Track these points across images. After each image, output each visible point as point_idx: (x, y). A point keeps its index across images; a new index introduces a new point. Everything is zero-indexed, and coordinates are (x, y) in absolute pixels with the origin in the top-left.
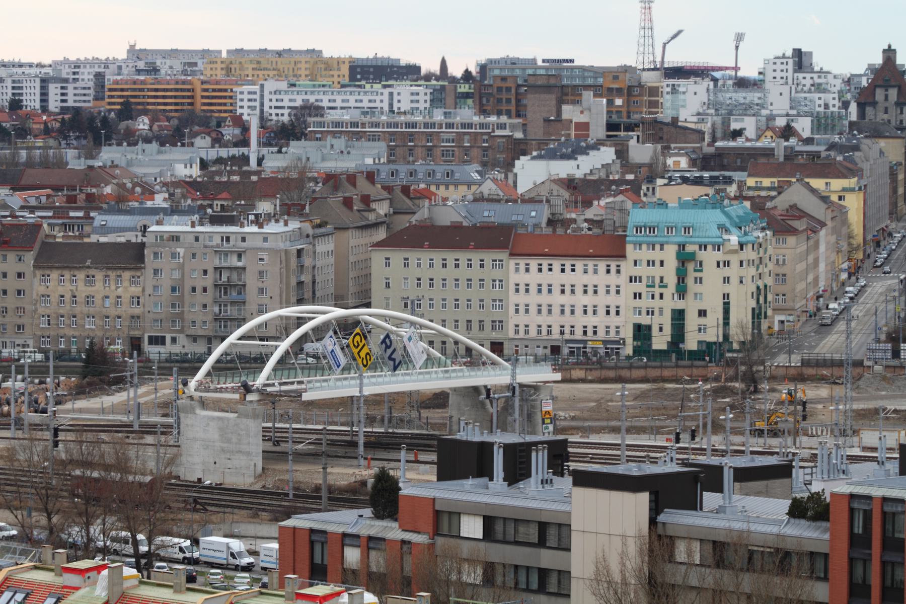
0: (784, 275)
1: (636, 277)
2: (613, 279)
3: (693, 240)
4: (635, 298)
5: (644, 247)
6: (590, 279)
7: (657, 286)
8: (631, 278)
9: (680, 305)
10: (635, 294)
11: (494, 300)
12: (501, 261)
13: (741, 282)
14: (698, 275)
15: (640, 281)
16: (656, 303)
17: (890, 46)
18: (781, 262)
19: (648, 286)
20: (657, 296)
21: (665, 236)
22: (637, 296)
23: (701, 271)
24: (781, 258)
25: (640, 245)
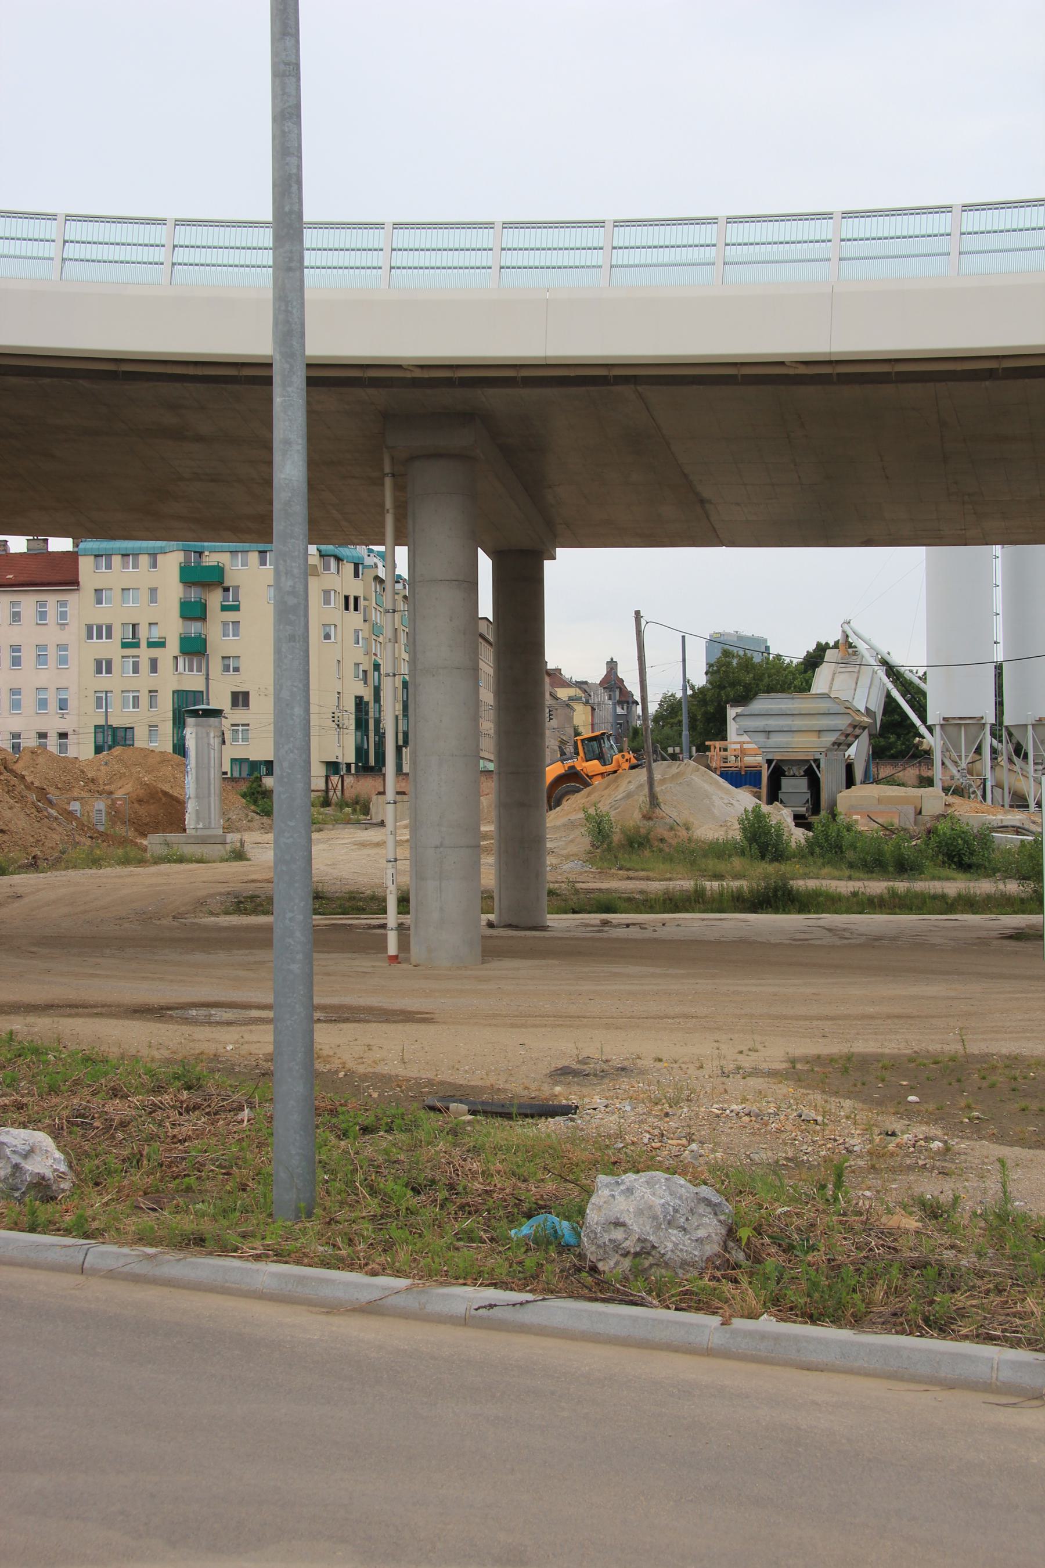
1: (99, 628)
2: (51, 635)
4: (99, 671)
5: (117, 560)
7: (144, 644)
8: (89, 628)
9: (194, 682)
10: (98, 663)
13: (327, 636)
14: (231, 616)
16: (145, 681)
17: (612, 659)
19: (125, 645)
20: (145, 666)
22: (104, 666)
23: (236, 608)
25: (109, 556)
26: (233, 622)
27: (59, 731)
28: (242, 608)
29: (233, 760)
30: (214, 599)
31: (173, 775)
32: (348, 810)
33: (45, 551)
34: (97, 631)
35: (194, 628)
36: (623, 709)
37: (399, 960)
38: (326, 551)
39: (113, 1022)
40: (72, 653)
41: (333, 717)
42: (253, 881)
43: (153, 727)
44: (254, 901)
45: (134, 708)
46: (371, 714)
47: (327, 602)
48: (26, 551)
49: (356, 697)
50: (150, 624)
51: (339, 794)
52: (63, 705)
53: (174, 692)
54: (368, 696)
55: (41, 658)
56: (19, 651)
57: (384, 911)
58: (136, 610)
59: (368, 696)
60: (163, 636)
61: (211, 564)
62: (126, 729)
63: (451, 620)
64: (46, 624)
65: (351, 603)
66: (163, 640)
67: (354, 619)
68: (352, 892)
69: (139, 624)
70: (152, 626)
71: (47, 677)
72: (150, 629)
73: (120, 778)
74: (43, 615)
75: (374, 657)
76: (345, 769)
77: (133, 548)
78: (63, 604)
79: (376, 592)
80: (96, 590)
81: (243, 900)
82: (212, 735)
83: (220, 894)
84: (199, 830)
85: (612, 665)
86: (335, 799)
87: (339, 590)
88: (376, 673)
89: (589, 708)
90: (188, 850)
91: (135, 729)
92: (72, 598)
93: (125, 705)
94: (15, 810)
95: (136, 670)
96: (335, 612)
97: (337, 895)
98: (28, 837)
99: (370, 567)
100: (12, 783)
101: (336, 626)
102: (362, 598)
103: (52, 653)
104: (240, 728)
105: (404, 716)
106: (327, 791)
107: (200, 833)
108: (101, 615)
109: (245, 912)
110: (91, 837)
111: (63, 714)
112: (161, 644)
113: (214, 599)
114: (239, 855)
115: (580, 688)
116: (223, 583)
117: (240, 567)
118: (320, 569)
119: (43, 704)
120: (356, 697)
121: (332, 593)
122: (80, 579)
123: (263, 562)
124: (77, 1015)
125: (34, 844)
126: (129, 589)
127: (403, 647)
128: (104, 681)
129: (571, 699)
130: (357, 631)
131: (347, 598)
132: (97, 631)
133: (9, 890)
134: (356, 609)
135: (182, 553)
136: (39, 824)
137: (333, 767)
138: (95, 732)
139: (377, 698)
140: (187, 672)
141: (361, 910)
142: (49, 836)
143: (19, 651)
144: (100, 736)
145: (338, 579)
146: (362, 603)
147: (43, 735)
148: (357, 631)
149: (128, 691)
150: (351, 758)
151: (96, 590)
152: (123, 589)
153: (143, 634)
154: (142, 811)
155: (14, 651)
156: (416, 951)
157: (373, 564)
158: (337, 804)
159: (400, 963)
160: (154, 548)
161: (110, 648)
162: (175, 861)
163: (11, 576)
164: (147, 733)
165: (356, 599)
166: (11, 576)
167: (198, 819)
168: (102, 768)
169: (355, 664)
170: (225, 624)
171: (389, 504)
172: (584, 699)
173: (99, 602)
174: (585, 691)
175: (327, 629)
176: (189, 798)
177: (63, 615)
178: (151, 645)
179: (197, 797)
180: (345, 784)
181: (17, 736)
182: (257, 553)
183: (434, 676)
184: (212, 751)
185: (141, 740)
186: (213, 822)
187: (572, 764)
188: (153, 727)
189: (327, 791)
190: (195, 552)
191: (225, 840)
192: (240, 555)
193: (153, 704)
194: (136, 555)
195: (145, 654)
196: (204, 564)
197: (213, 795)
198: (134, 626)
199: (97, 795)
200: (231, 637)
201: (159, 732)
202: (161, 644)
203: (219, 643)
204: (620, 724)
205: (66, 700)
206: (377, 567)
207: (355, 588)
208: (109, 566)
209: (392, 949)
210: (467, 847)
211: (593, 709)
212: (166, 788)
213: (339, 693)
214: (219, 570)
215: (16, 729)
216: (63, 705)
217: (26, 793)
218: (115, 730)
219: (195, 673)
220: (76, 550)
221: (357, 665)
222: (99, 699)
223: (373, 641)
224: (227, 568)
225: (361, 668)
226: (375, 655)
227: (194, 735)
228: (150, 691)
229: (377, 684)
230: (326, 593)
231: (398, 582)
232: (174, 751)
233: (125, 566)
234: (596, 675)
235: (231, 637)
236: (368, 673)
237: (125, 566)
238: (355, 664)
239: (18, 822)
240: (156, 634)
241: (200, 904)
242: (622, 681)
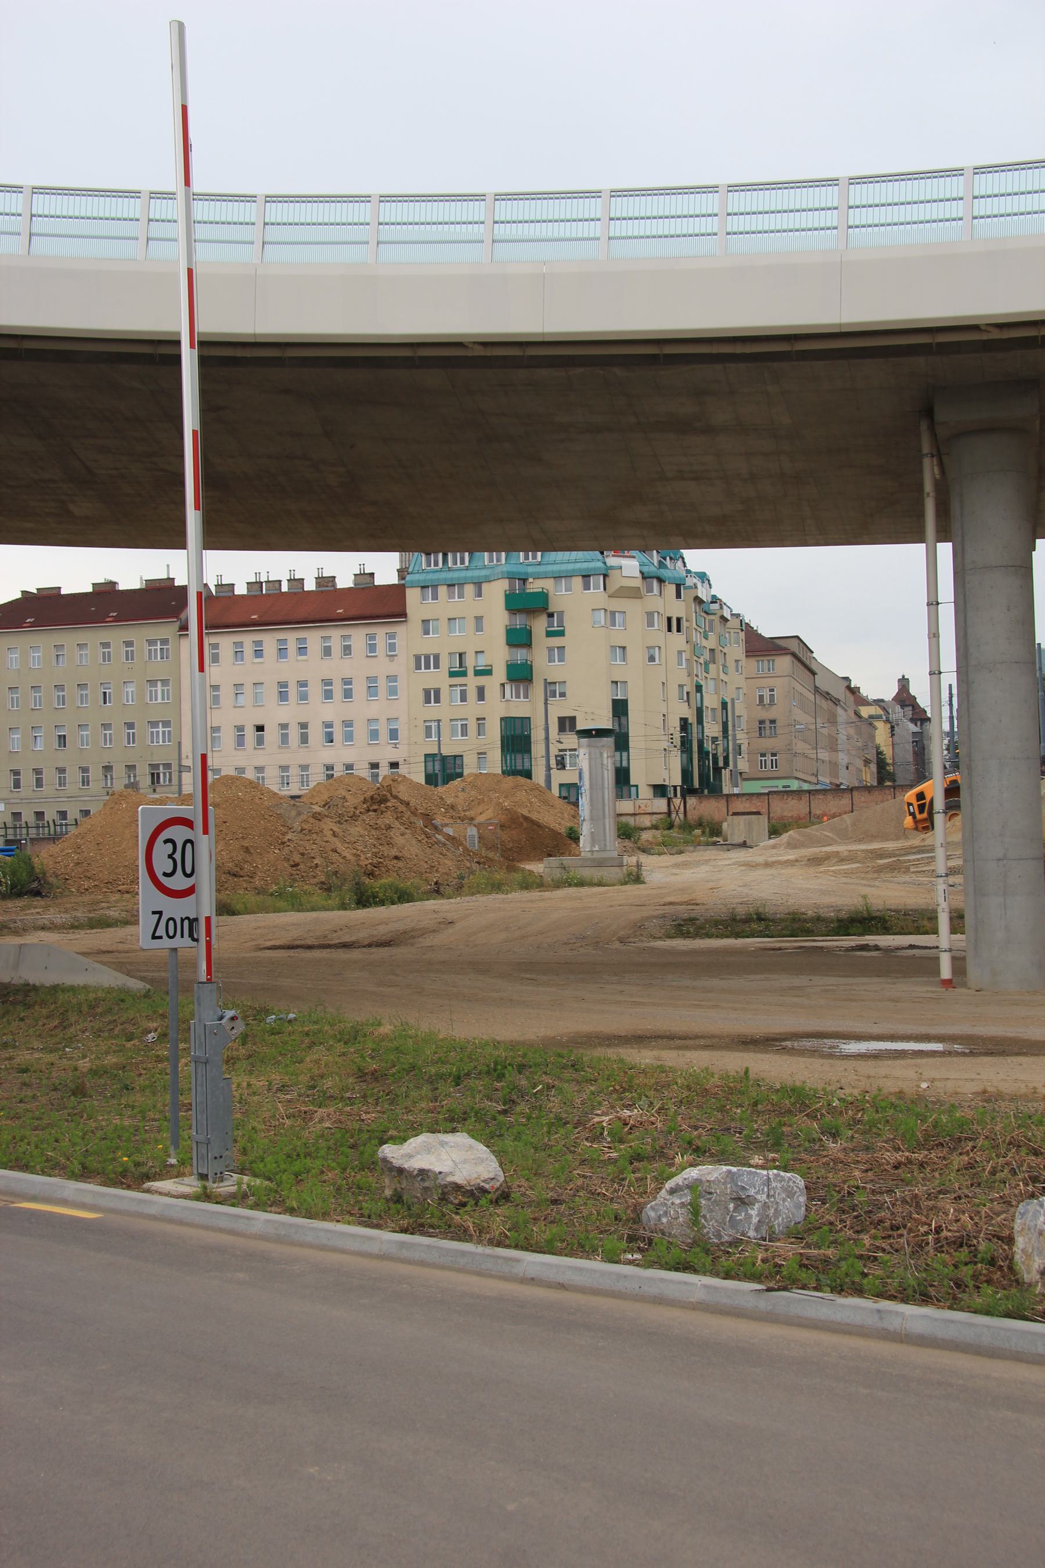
0: (773, 722)
1: (427, 658)
2: (381, 667)
3: (542, 569)
4: (428, 700)
5: (442, 590)
6: (337, 668)
7: (471, 672)
8: (418, 658)
9: (519, 708)
10: (427, 693)
11: (154, 724)
12: (165, 642)
13: (652, 659)
14: (556, 641)
15: (437, 666)
16: (472, 709)
17: (903, 676)
18: (767, 701)
19: (452, 674)
20: (472, 694)
21: (485, 567)
22: (432, 696)
23: (561, 634)
24: (766, 694)
25: (435, 587)
26: (558, 648)
27: (391, 760)
28: (566, 633)
29: (561, 785)
30: (539, 625)
31: (529, 800)
32: (698, 832)
33: (371, 585)
34: (425, 661)
35: (520, 655)
36: (916, 725)
37: (954, 985)
38: (648, 572)
39: (724, 1053)
40: (401, 684)
41: (672, 739)
42: (671, 903)
43: (482, 755)
44: (694, 924)
45: (462, 736)
46: (695, 735)
47: (650, 624)
48: (352, 586)
49: (681, 719)
50: (477, 652)
51: (682, 816)
52: (394, 734)
53: (502, 719)
54: (692, 719)
55: (372, 690)
56: (350, 683)
57: (935, 931)
58: (464, 639)
59: (692, 719)
60: (490, 663)
61: (535, 590)
62: (455, 756)
63: (1008, 610)
64: (376, 656)
65: (674, 625)
66: (490, 668)
67: (677, 640)
68: (794, 913)
69: (465, 653)
70: (479, 655)
71: (379, 708)
72: (476, 657)
73: (479, 803)
74: (372, 648)
75: (695, 678)
76: (672, 792)
77: (459, 579)
78: (392, 636)
79: (696, 613)
80: (423, 621)
81: (682, 923)
82: (605, 755)
83: (656, 917)
84: (595, 853)
85: (904, 683)
86: (677, 822)
87: (661, 611)
88: (699, 695)
89: (889, 726)
90: (587, 873)
91: (465, 758)
92: (400, 630)
93: (453, 733)
94: (407, 836)
95: (463, 698)
96: (658, 634)
97: (778, 916)
98: (422, 863)
99: (690, 587)
100: (400, 809)
101: (660, 648)
102: (684, 619)
103: (382, 684)
104: (568, 753)
105: (724, 737)
106: (669, 813)
107: (596, 855)
108: (428, 645)
109: (687, 935)
110: (478, 863)
111: (396, 744)
112: (487, 672)
113: (539, 625)
114: (636, 878)
115: (879, 706)
116: (547, 609)
117: (564, 593)
118: (643, 591)
119: (374, 734)
120: (681, 719)
121: (656, 615)
122: (408, 611)
123: (587, 587)
124: (687, 1048)
125: (428, 870)
126: (455, 619)
127: (721, 667)
128: (433, 711)
129: (871, 717)
130: (680, 653)
131: (669, 619)
132: (425, 661)
133: (435, 916)
134: (679, 630)
135: (507, 581)
136: (431, 850)
137: (660, 790)
138: (425, 762)
139: (700, 721)
140: (514, 699)
141: (809, 932)
142: (441, 861)
143: (350, 683)
144: (430, 764)
145: (660, 600)
146: (684, 624)
147: (375, 766)
148: (680, 653)
149: (457, 720)
150: (677, 780)
151: (423, 621)
152: (449, 619)
153: (470, 662)
154: (505, 836)
155: (326, 684)
156: (974, 974)
157: (692, 585)
158: (680, 827)
159: (954, 987)
160: (479, 577)
161: (438, 678)
162: (577, 885)
163: (341, 611)
164: (476, 760)
165: (679, 620)
166: (341, 611)
167: (593, 842)
168: (460, 794)
169: (679, 685)
170: (551, 650)
171: (928, 487)
172: (884, 717)
173: (426, 632)
174: (884, 709)
175: (652, 651)
176: (584, 820)
177: (392, 647)
178: (478, 673)
179: (592, 819)
180: (688, 806)
181: (330, 768)
182: (581, 578)
183: (991, 671)
184: (606, 772)
185: (470, 767)
186: (608, 844)
187: (954, 778)
188: (482, 755)
189: (669, 813)
190: (519, 579)
191: (622, 862)
192: (563, 580)
193: (481, 732)
194: (461, 585)
195: (472, 682)
196: (528, 591)
197: (607, 817)
198: (460, 655)
199: (458, 821)
200: (557, 663)
201: (488, 759)
202: (487, 672)
203: (544, 667)
204: (916, 742)
205: (397, 730)
206: (696, 587)
207: (677, 609)
208: (435, 597)
209: (946, 973)
210: (1033, 859)
211: (892, 728)
212: (525, 812)
213: (664, 715)
214: (543, 597)
215: (349, 761)
216: (394, 734)
217: (413, 819)
218: (444, 759)
219: (522, 699)
220: (403, 582)
221: (681, 686)
222: (428, 729)
223: (695, 663)
224: (551, 594)
225: (686, 689)
226: (697, 676)
227: (587, 756)
228: (478, 719)
229: (699, 705)
230: (650, 615)
231: (716, 602)
232: (427, 783)
233: (451, 596)
234: (889, 692)
235: (557, 663)
236: (690, 694)
237: (451, 596)
238: (679, 685)
239: (412, 849)
240: (482, 662)
241: (639, 927)
242: (914, 698)
